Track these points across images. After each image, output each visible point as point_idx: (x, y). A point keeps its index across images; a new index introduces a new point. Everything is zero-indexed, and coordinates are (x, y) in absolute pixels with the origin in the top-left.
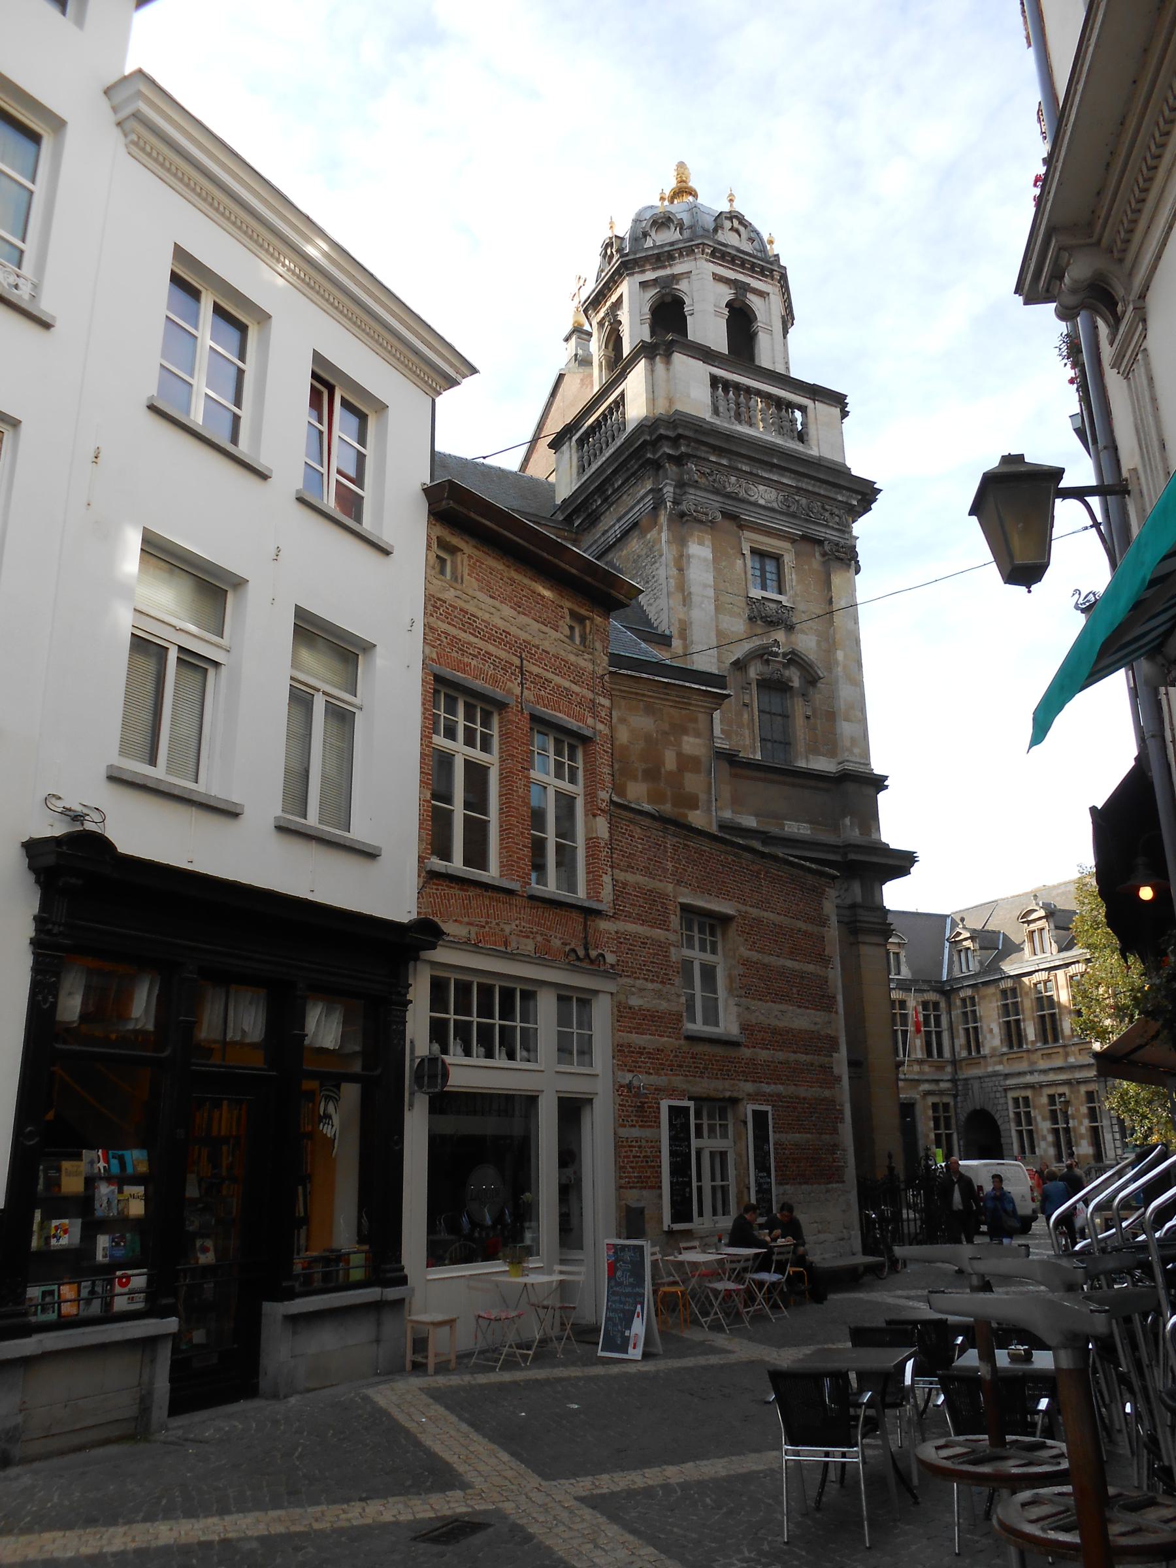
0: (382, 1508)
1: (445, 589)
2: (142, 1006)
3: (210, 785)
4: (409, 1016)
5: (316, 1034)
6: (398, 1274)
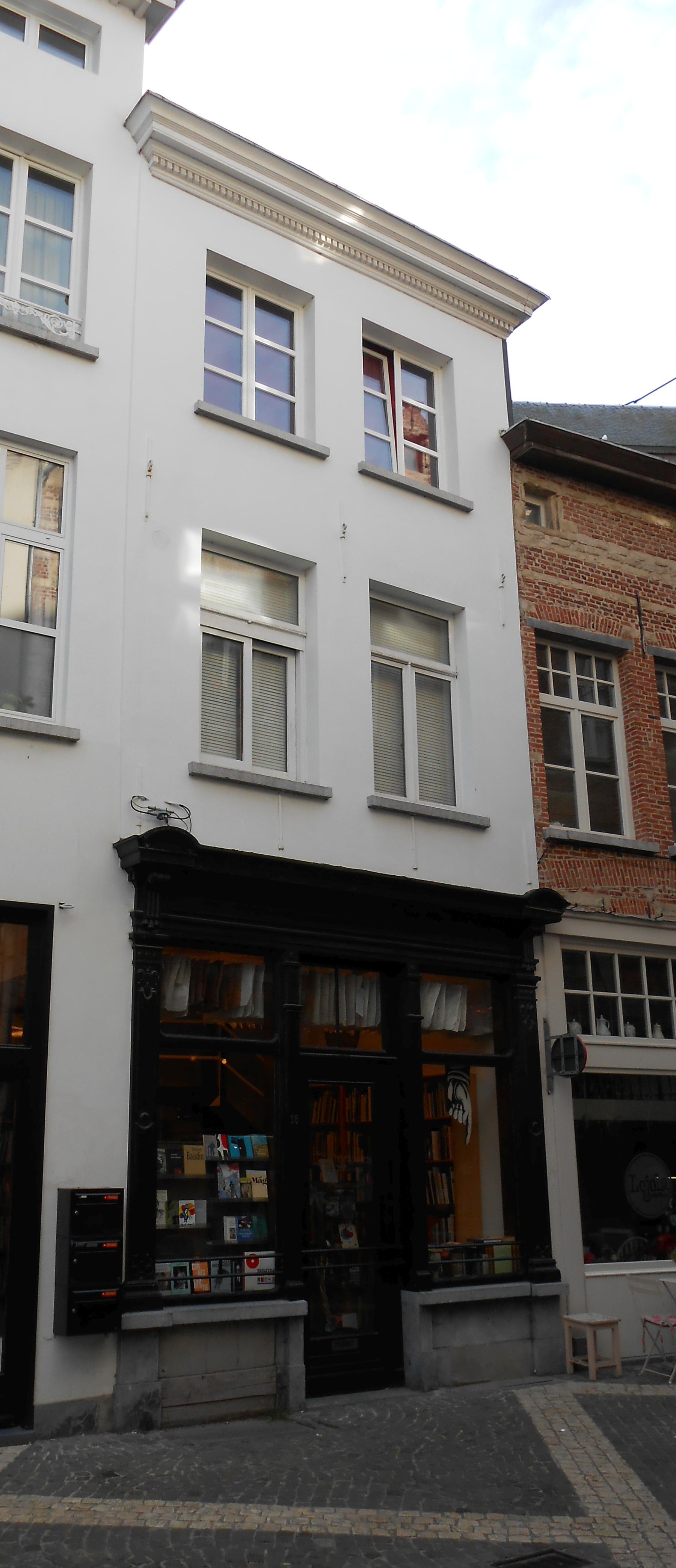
0: (476, 1524)
1: (538, 538)
2: (249, 992)
3: (299, 773)
4: (540, 994)
5: (436, 1016)
6: (549, 1268)
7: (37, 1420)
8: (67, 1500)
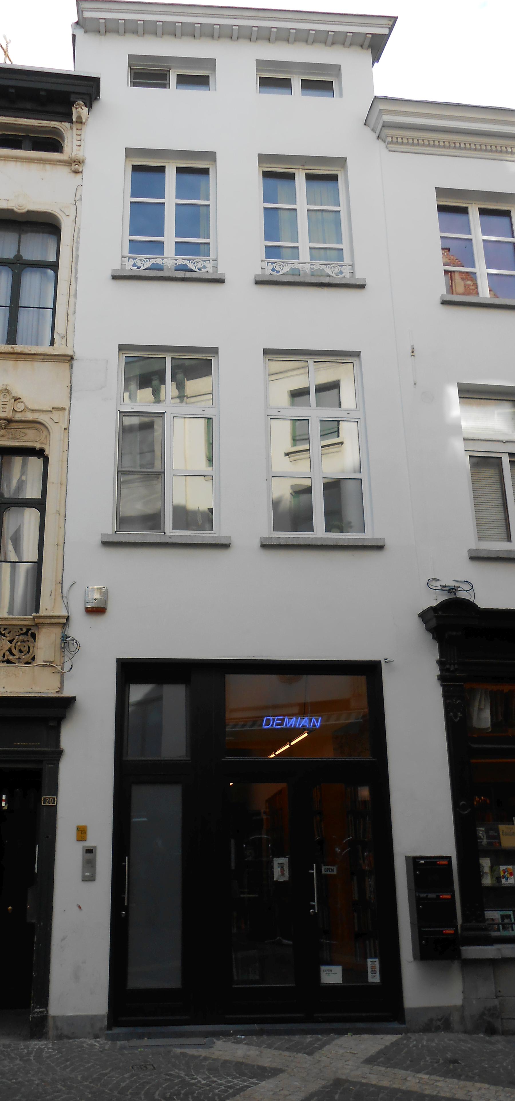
7: (407, 1017)
8: (420, 1075)
